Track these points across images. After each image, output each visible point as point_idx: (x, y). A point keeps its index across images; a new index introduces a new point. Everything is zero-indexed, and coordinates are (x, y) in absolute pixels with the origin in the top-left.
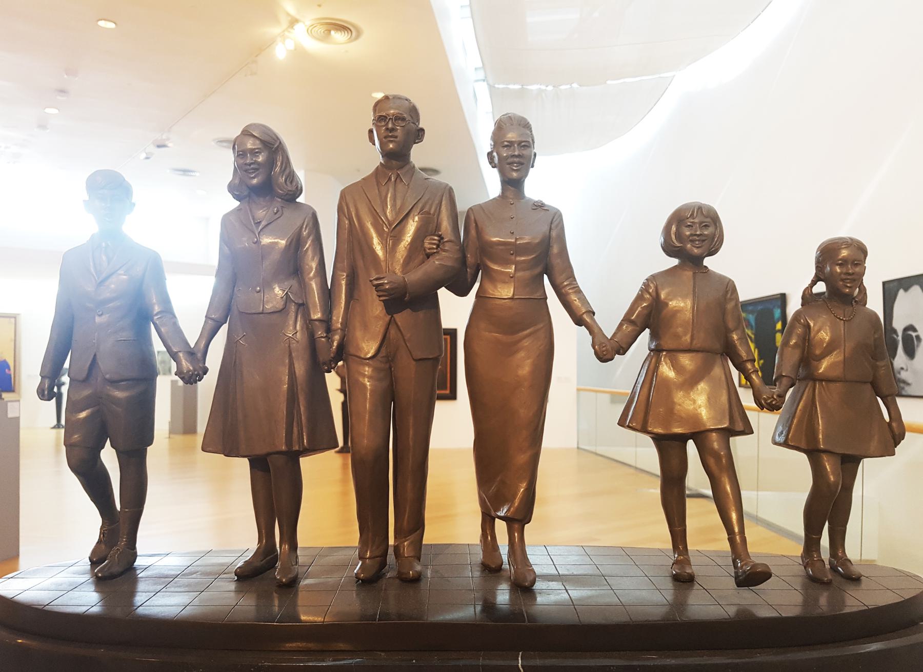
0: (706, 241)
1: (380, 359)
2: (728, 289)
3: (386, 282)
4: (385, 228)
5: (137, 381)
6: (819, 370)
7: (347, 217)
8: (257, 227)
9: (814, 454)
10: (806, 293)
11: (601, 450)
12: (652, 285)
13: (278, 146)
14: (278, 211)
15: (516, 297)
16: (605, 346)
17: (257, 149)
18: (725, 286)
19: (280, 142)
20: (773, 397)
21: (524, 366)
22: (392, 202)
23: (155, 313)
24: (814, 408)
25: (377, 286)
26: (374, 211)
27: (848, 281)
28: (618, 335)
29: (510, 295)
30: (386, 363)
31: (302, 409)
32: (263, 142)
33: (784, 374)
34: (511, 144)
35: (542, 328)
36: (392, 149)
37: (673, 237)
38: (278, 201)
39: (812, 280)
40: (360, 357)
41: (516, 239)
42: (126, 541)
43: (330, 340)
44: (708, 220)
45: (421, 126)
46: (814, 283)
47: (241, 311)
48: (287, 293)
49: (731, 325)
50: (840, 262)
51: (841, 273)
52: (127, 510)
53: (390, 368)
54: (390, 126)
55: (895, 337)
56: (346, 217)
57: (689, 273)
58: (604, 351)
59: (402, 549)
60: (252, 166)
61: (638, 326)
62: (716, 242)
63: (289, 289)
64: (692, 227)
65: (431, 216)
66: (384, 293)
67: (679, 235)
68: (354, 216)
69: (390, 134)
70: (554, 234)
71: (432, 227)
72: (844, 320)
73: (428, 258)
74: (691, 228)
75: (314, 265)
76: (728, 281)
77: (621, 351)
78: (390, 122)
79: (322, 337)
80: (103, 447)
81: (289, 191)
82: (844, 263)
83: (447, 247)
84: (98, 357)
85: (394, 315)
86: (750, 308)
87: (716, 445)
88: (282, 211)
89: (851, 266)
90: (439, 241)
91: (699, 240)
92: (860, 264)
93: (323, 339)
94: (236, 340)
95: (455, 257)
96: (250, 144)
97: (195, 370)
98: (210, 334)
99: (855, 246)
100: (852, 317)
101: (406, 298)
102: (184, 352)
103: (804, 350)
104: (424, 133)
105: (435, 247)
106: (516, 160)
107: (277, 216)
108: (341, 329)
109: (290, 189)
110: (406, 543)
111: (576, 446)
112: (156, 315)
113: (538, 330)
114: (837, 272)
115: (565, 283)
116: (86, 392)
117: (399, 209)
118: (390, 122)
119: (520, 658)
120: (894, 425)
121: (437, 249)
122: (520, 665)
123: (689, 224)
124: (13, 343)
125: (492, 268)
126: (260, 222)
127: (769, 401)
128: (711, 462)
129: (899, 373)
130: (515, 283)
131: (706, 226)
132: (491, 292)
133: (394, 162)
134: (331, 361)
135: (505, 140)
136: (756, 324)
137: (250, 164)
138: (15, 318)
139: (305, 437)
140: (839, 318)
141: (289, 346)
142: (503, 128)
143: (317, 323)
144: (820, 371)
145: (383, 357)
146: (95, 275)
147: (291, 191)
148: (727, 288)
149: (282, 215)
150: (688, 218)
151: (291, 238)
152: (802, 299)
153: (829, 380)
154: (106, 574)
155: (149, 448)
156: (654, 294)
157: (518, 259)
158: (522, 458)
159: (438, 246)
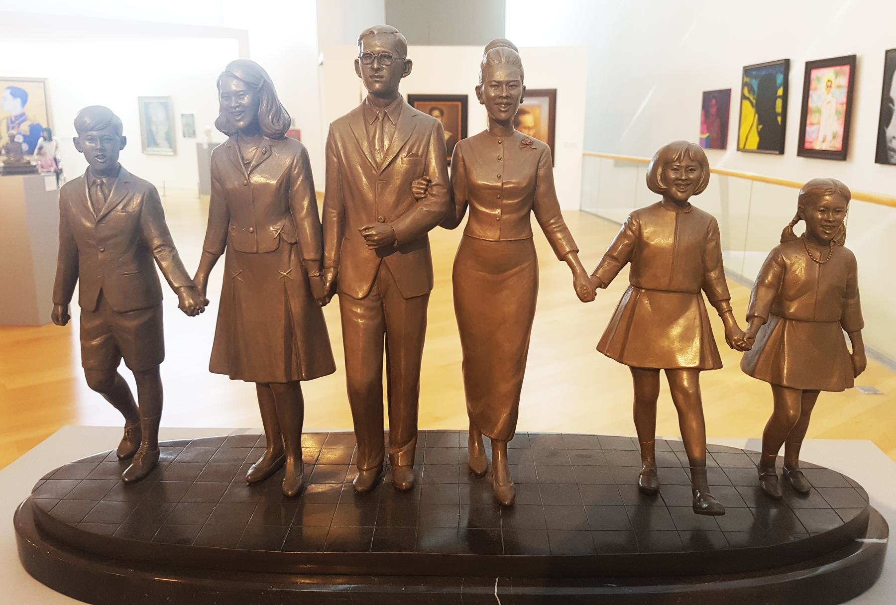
0: (691, 185)
1: (371, 298)
2: (709, 229)
3: (374, 233)
4: (373, 172)
5: (142, 310)
6: (790, 310)
7: (336, 155)
8: (246, 168)
9: (777, 388)
10: (786, 231)
11: (602, 212)
12: (634, 223)
13: (263, 86)
14: (266, 151)
15: (502, 240)
16: (587, 289)
17: (242, 91)
18: (707, 227)
19: (265, 80)
20: (743, 340)
21: (509, 304)
22: (380, 143)
23: (154, 247)
24: (782, 345)
25: (366, 237)
26: (363, 154)
27: (828, 228)
28: (600, 272)
29: (496, 237)
30: (378, 300)
31: (299, 343)
32: (247, 84)
33: (756, 315)
34: (499, 84)
35: (527, 267)
36: (378, 89)
37: (659, 178)
38: (266, 139)
39: (793, 220)
40: (352, 297)
41: (503, 184)
42: (147, 444)
43: (323, 278)
44: (693, 164)
45: (408, 57)
46: (795, 222)
47: (237, 250)
48: (279, 233)
49: (710, 264)
50: (822, 208)
51: (822, 219)
52: (146, 418)
53: (382, 304)
54: (375, 66)
55: (891, 105)
56: (335, 156)
57: (673, 214)
58: (585, 294)
59: (396, 460)
60: (237, 109)
61: (619, 262)
62: (701, 184)
63: (282, 229)
64: (678, 170)
65: (419, 158)
66: (374, 243)
67: (665, 178)
68: (342, 154)
69: (376, 75)
70: (541, 172)
71: (420, 169)
72: (820, 263)
73: (417, 201)
74: (676, 171)
75: (306, 203)
76: (710, 220)
77: (603, 286)
78: (376, 61)
79: (316, 276)
80: (119, 364)
81: (276, 130)
82: (826, 209)
83: (435, 191)
84: (104, 291)
85: (384, 258)
86: (754, 73)
87: (686, 383)
88: (271, 151)
89: (832, 213)
90: (427, 185)
91: (684, 185)
92: (841, 211)
93: (317, 278)
94: (233, 277)
95: (443, 200)
96: (234, 86)
97: (196, 304)
98: (207, 265)
99: (838, 193)
100: (828, 260)
101: (395, 245)
102: (185, 287)
103: (778, 289)
104: (411, 65)
105: (422, 192)
106: (505, 101)
107: (266, 156)
108: (334, 267)
109: (277, 128)
110: (400, 453)
111: (578, 208)
112: (156, 249)
113: (524, 269)
114: (818, 218)
115: (552, 221)
116: (97, 322)
117: (386, 150)
118: (376, 61)
119: (496, 587)
120: (857, 358)
121: (425, 193)
122: (496, 594)
123: (675, 167)
124: (44, 107)
125: (478, 210)
126: (249, 163)
127: (739, 343)
128: (680, 397)
129: (891, 141)
130: (501, 226)
131: (691, 170)
132: (478, 233)
133: (381, 100)
134: (325, 297)
135: (493, 79)
136: (759, 88)
137: (235, 108)
138: (44, 82)
139: (303, 369)
140: (815, 261)
141: (284, 285)
142: (492, 66)
143: (310, 262)
144: (792, 311)
145: (375, 296)
146: (94, 214)
147: (278, 130)
148: (708, 229)
149: (270, 155)
150: (674, 162)
151: (281, 180)
152: (782, 236)
153: (799, 320)
154: (133, 478)
155: (161, 365)
156: (637, 233)
157: (505, 201)
158: (505, 387)
159: (426, 190)
